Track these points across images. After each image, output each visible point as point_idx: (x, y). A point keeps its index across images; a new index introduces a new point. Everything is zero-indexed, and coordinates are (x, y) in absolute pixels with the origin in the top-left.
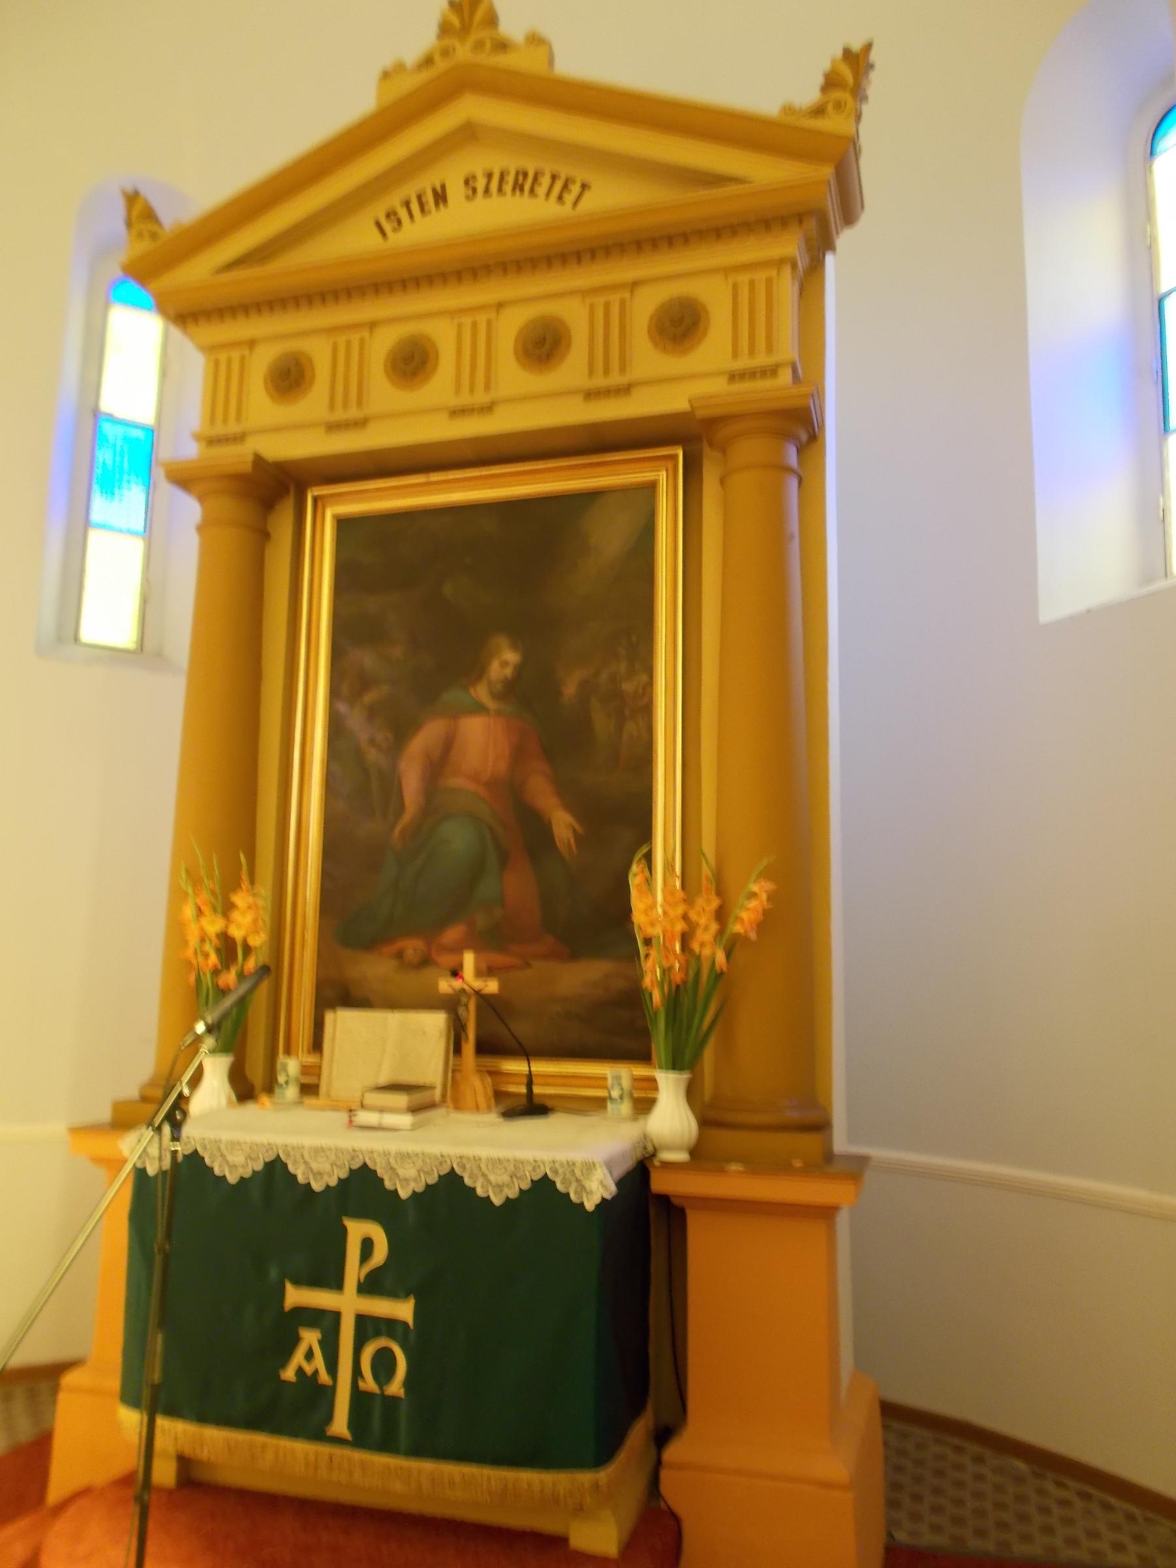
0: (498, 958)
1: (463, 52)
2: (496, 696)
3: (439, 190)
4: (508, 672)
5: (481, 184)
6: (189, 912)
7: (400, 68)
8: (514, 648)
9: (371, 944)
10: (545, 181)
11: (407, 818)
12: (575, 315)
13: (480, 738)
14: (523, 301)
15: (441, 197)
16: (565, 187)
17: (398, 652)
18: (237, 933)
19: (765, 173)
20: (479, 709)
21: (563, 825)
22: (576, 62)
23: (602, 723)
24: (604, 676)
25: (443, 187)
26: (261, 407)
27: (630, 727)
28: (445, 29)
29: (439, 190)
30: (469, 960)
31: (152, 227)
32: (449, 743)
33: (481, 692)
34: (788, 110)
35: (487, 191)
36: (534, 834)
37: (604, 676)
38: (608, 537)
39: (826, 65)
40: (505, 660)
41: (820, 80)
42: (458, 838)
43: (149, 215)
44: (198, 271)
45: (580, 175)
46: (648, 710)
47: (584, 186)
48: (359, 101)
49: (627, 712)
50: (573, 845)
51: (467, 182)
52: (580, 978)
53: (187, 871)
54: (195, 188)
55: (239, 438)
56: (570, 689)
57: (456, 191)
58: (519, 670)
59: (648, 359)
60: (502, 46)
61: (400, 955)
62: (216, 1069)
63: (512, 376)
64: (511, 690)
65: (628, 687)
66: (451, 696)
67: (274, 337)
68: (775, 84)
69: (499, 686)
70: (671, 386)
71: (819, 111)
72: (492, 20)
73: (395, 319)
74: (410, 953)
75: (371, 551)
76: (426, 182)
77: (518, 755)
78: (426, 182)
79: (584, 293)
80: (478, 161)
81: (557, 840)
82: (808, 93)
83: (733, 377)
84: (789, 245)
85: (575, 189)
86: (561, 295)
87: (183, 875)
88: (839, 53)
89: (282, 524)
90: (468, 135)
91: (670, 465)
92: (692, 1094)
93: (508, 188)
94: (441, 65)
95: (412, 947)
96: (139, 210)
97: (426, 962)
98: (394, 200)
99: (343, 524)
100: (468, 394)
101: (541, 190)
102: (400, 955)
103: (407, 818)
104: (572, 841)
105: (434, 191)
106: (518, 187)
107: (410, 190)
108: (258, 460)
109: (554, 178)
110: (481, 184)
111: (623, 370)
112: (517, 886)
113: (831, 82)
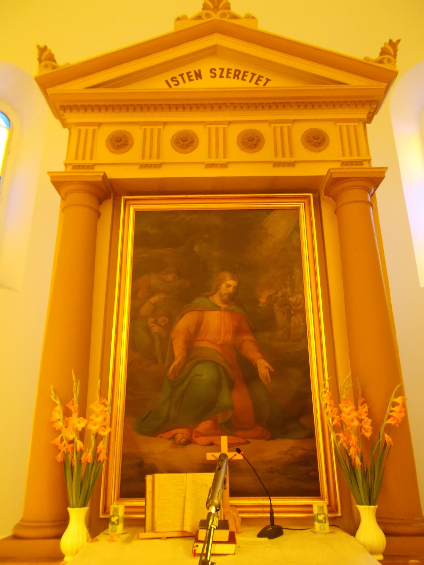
0: (236, 440)
1: (216, 16)
2: (225, 302)
3: (198, 72)
4: (231, 290)
5: (218, 72)
6: (58, 414)
7: (184, 18)
8: (233, 279)
9: (155, 433)
10: (249, 76)
11: (175, 363)
12: (265, 131)
13: (216, 322)
14: (239, 123)
15: (198, 75)
16: (258, 79)
17: (170, 277)
18: (94, 428)
19: (354, 82)
20: (216, 308)
21: (263, 367)
22: (266, 25)
23: (280, 318)
24: (280, 294)
25: (200, 71)
26: (103, 154)
27: (294, 319)
28: (205, 7)
29: (198, 72)
30: (224, 440)
31: (53, 63)
32: (199, 325)
33: (216, 299)
34: (366, 59)
35: (221, 76)
36: (250, 375)
37: (280, 294)
38: (277, 229)
39: (383, 46)
40: (228, 284)
41: (379, 51)
42: (205, 374)
43: (51, 58)
44: (78, 86)
45: (266, 75)
46: (303, 311)
47: (268, 80)
48: (168, 28)
49: (292, 312)
50: (269, 378)
51: (211, 71)
52: (278, 450)
53: (54, 390)
54: (67, 56)
55: (92, 166)
56: (263, 300)
57: (206, 74)
58: (237, 288)
59: (302, 152)
60: (235, 17)
61: (173, 438)
62: (77, 516)
63: (236, 153)
64: (232, 299)
65: (292, 299)
66: (200, 301)
67: (112, 123)
68: (367, 50)
69: (226, 297)
70: (315, 166)
71: (381, 61)
72: (228, 7)
73: (176, 122)
74: (179, 437)
75: (153, 234)
76: (193, 68)
77: (238, 331)
78: (193, 68)
79: (271, 122)
80: (217, 64)
81: (260, 376)
82: (375, 55)
83: (343, 163)
84: (363, 114)
85: (264, 80)
86: (261, 122)
87: (53, 393)
88: (387, 41)
89: (107, 210)
90: (213, 51)
91: (306, 201)
92: (382, 521)
93: (231, 75)
94: (206, 20)
95: (181, 434)
96: (45, 56)
97: (189, 442)
98: (175, 73)
99: (138, 214)
100: (219, 154)
101: (248, 78)
102: (173, 438)
103: (175, 363)
104: (268, 375)
105: (195, 72)
106: (236, 76)
107: (184, 70)
108: (105, 176)
109: (253, 75)
110: (218, 72)
111: (291, 156)
112: (237, 399)
113: (384, 52)
